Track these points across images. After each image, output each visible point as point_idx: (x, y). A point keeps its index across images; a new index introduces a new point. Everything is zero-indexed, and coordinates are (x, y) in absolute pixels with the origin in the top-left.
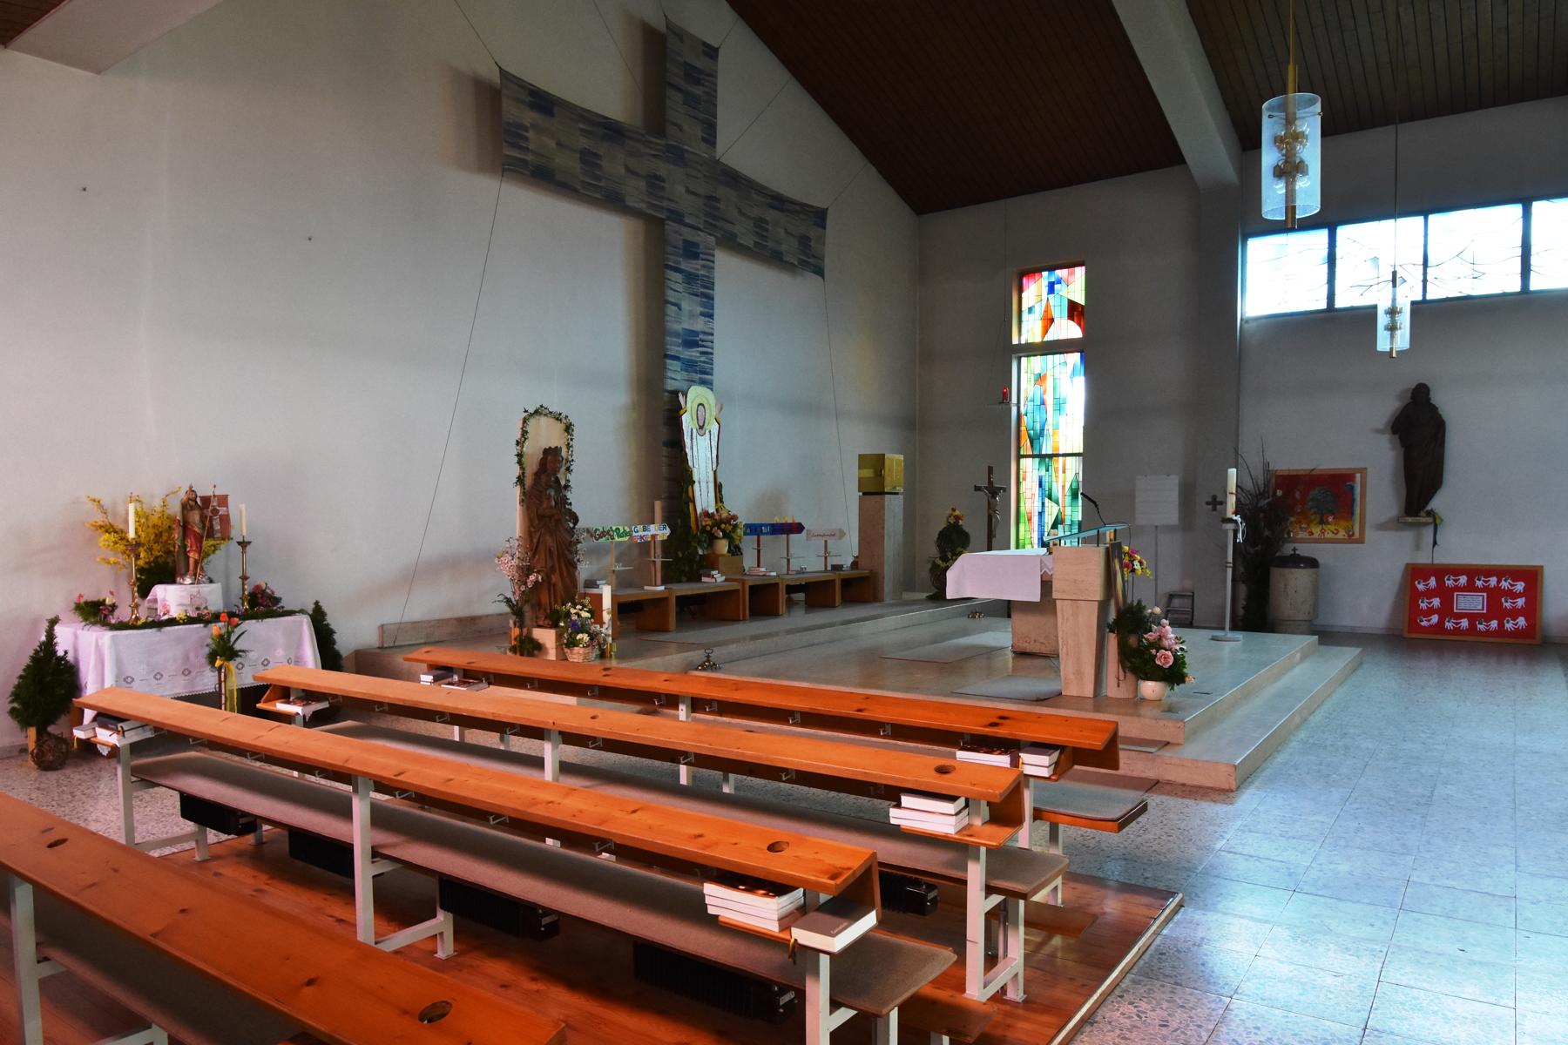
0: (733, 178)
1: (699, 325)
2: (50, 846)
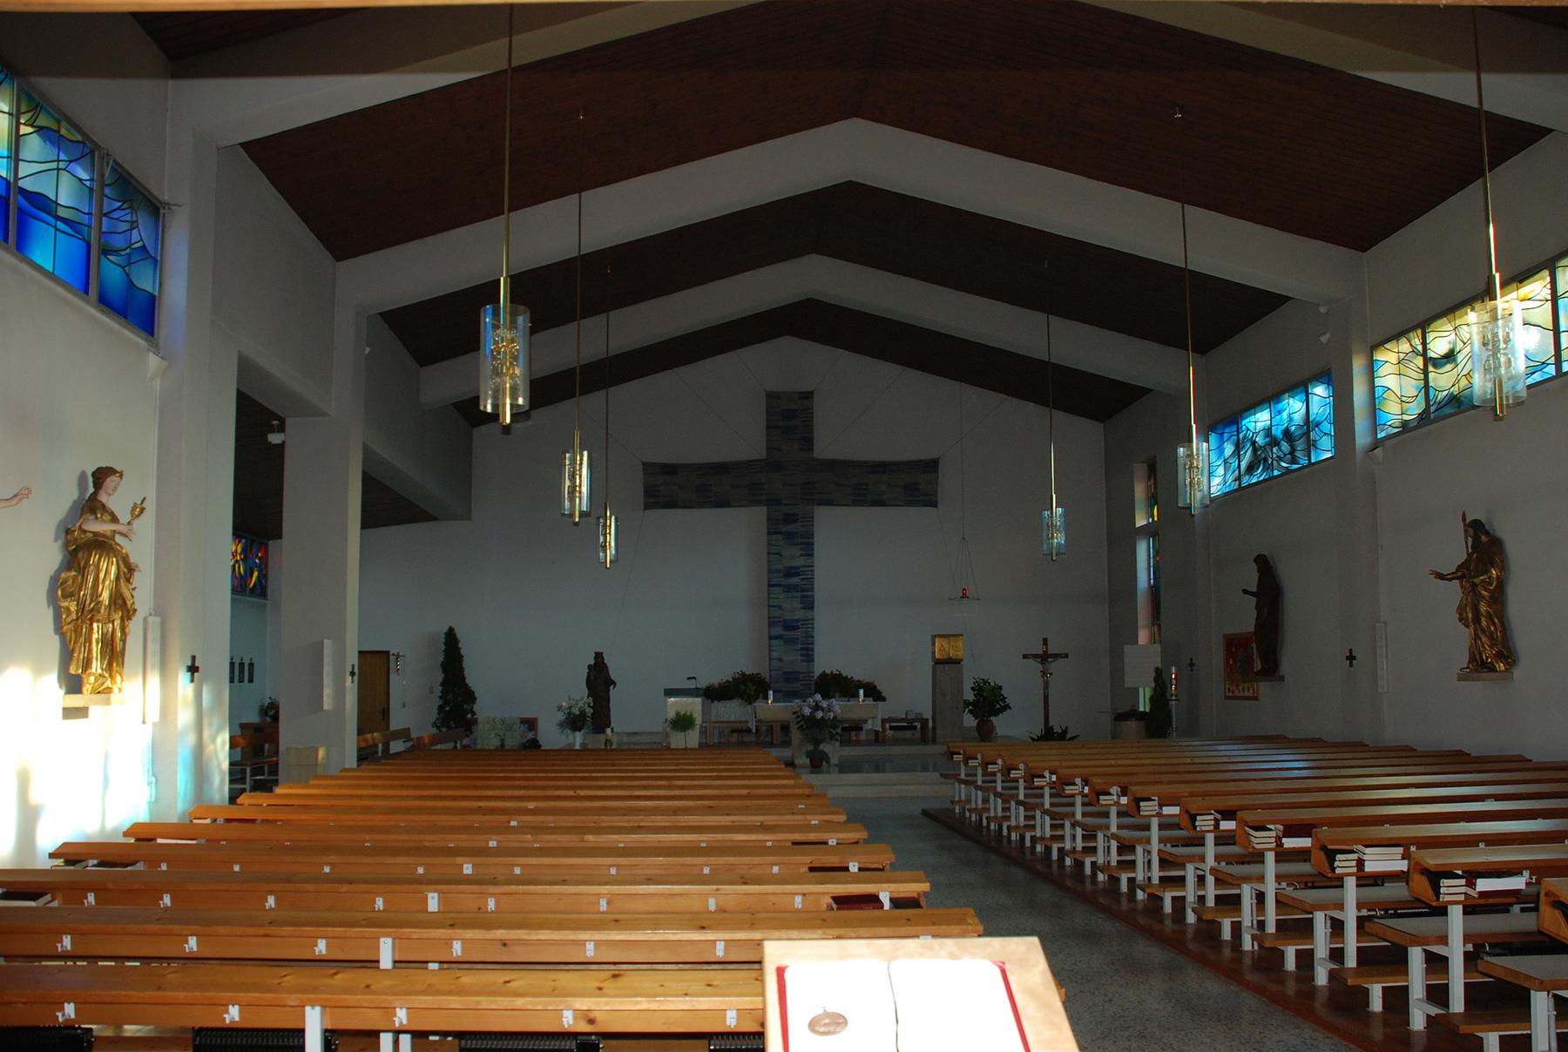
0: (832, 465)
1: (799, 562)
2: (1066, 656)
